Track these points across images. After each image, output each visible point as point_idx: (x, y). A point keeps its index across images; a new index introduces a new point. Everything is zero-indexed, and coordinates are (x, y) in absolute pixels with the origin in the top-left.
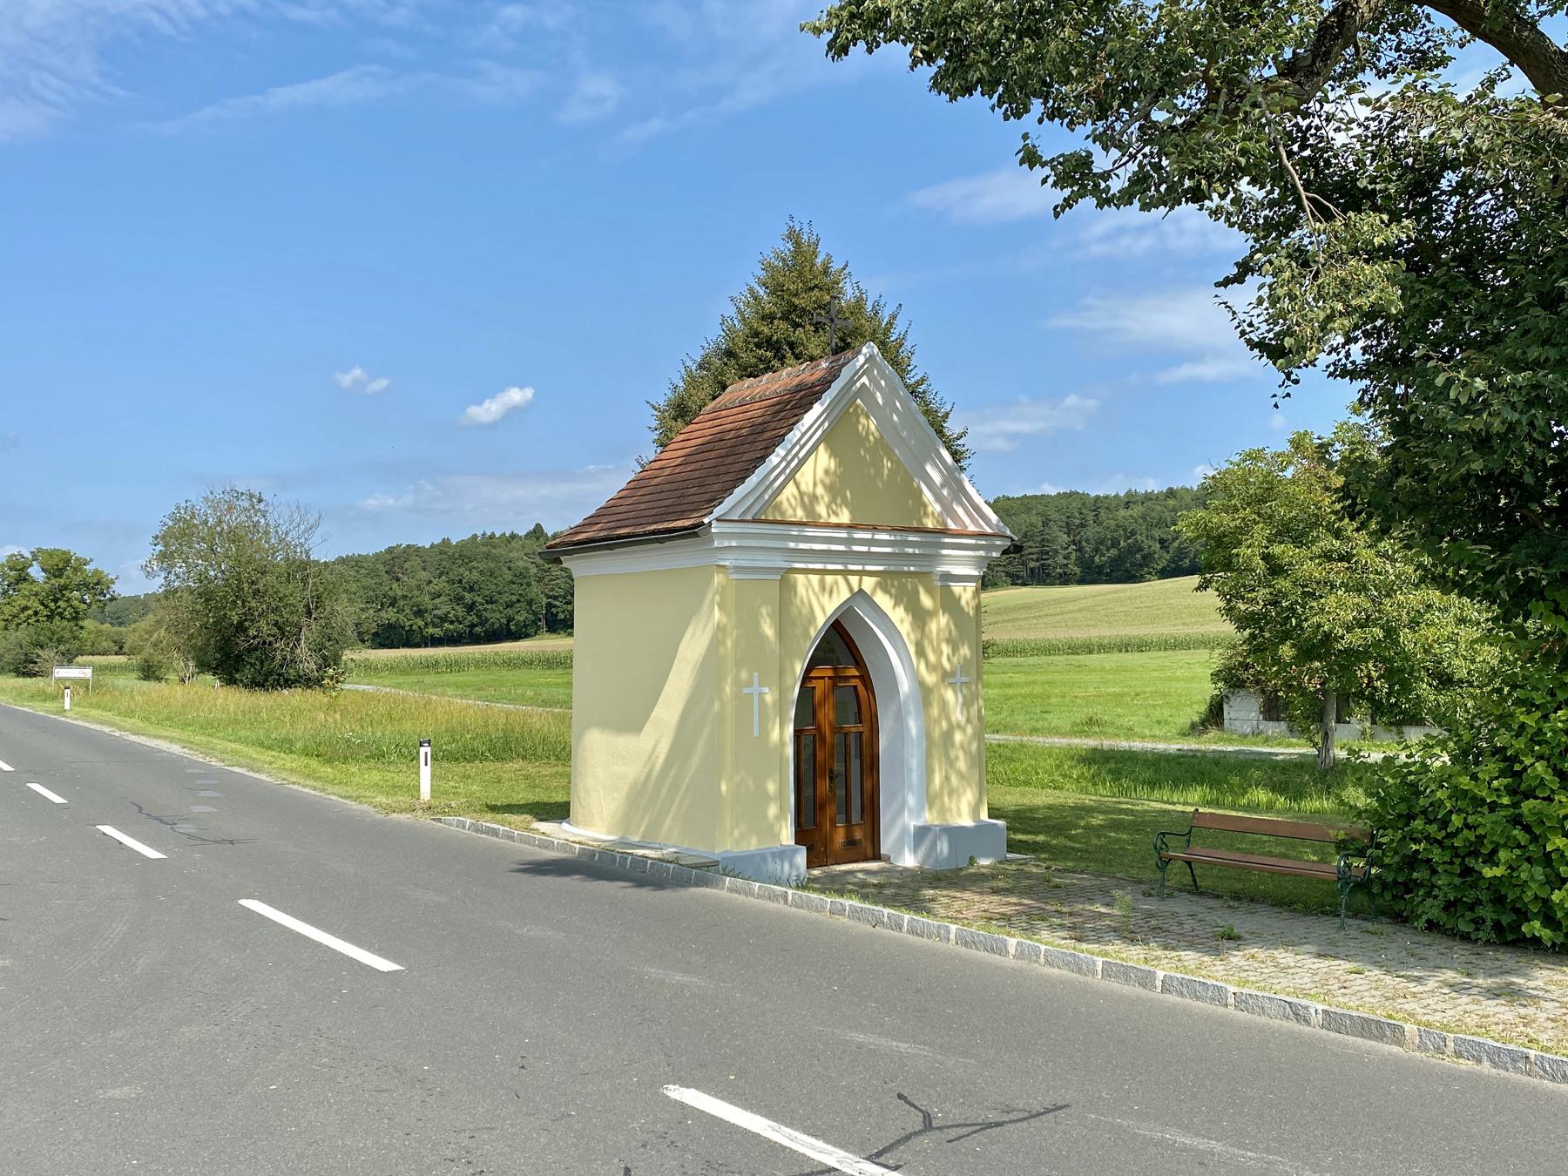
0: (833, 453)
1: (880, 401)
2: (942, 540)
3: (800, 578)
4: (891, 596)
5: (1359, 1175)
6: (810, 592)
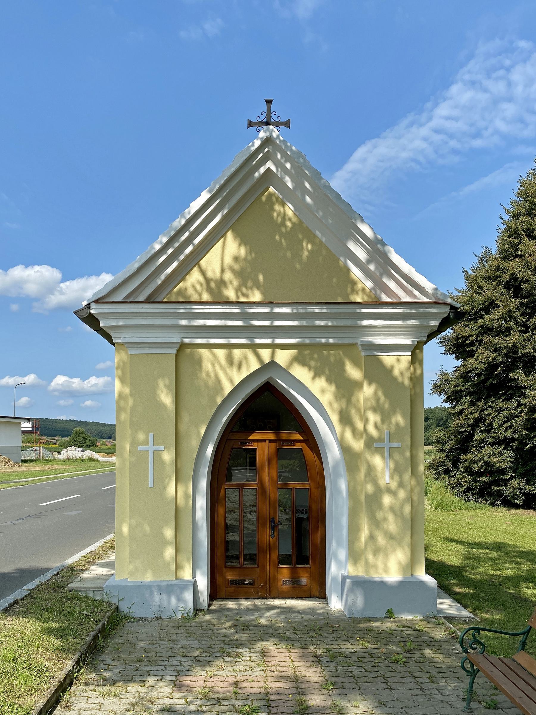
0: (243, 240)
1: (290, 185)
2: (358, 311)
3: (205, 353)
4: (310, 368)
5: (529, 82)
6: (217, 367)
